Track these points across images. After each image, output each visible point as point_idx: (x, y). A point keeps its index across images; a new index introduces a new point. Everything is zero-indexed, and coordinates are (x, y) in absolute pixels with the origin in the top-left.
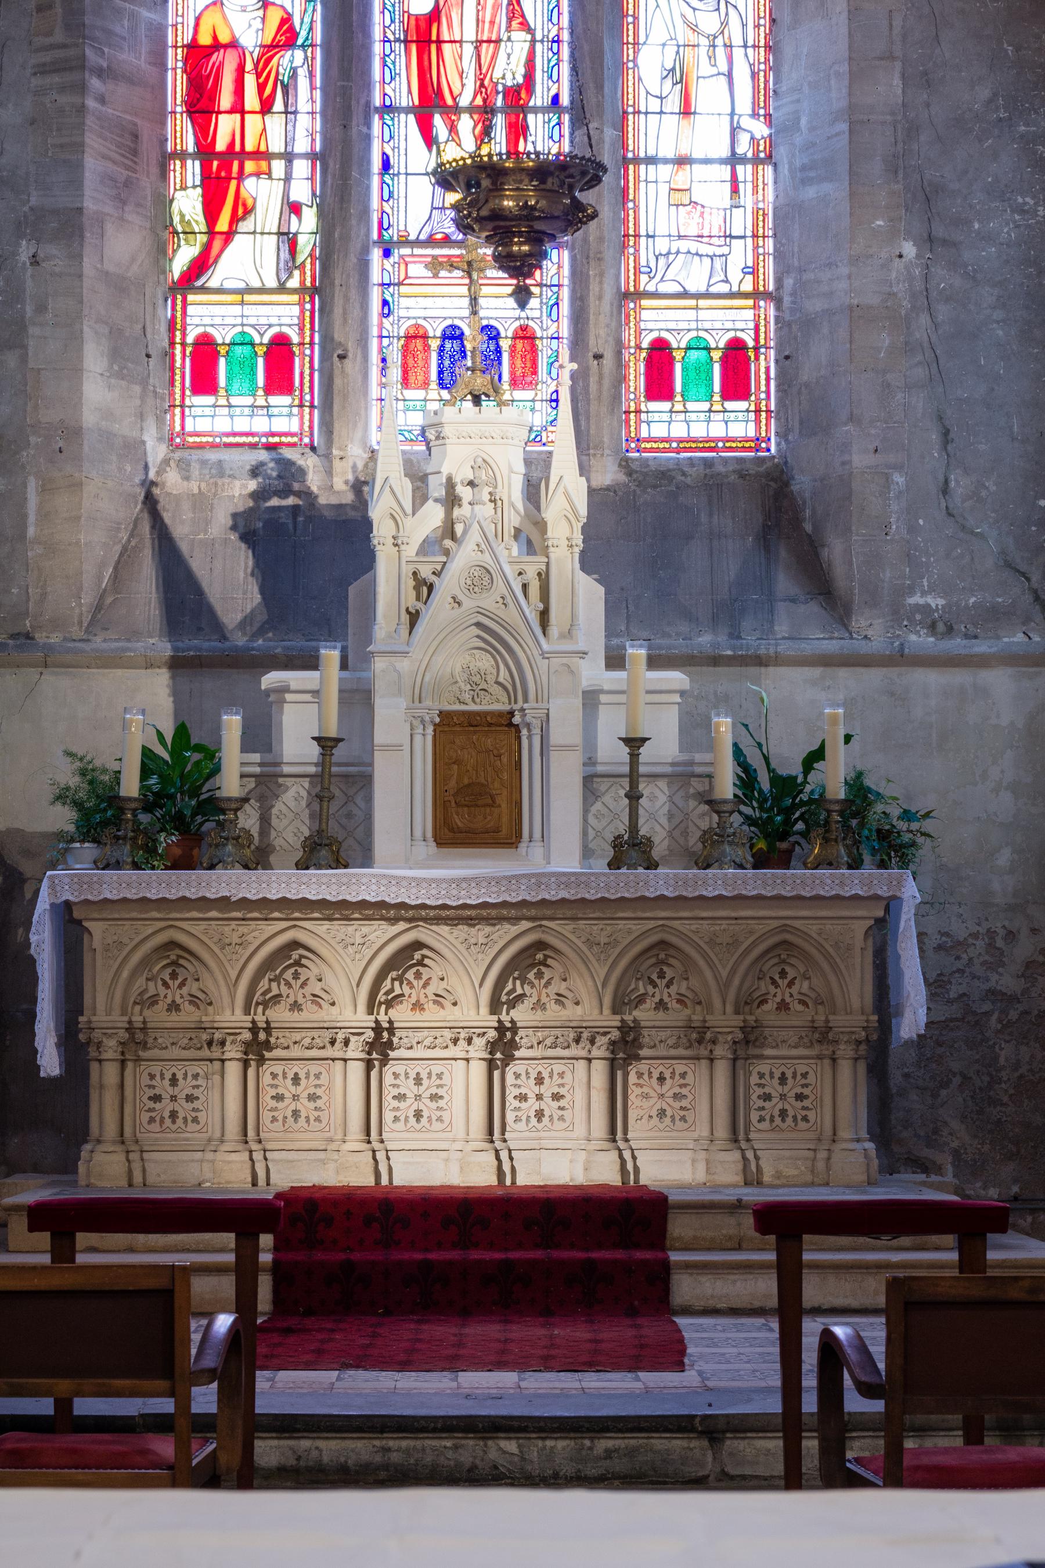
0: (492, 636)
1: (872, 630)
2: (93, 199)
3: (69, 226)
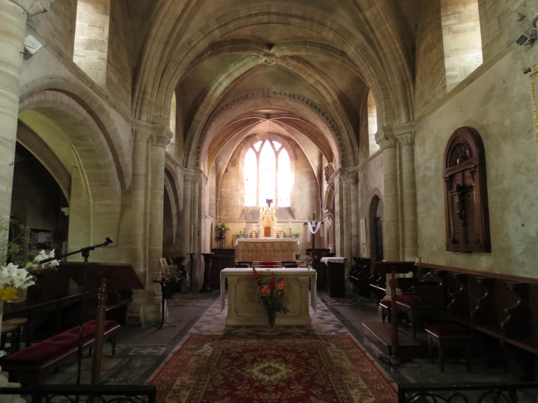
0: (269, 222)
1: (297, 220)
2: (239, 188)
3: (238, 190)
